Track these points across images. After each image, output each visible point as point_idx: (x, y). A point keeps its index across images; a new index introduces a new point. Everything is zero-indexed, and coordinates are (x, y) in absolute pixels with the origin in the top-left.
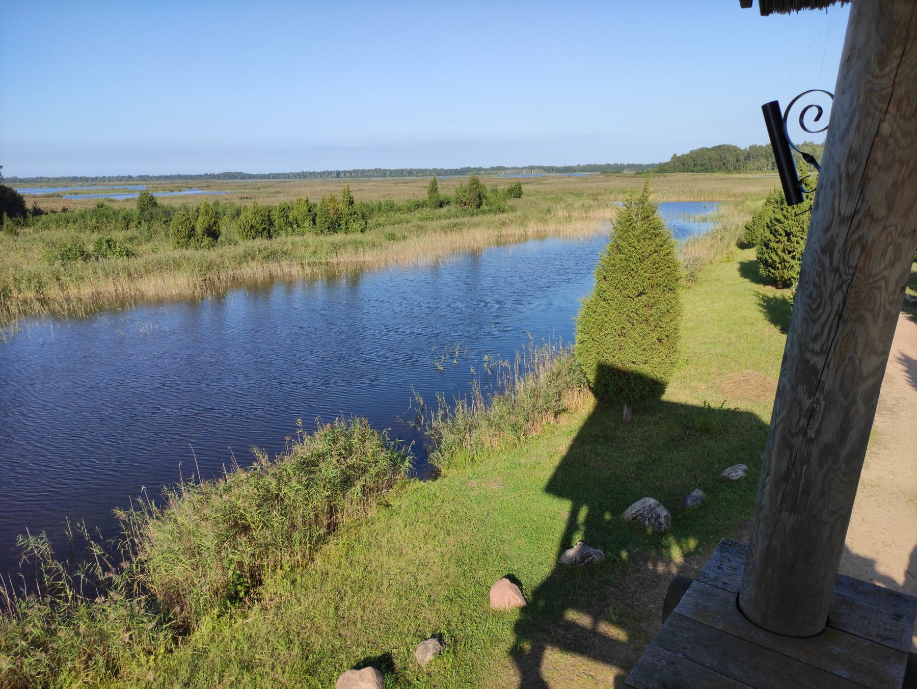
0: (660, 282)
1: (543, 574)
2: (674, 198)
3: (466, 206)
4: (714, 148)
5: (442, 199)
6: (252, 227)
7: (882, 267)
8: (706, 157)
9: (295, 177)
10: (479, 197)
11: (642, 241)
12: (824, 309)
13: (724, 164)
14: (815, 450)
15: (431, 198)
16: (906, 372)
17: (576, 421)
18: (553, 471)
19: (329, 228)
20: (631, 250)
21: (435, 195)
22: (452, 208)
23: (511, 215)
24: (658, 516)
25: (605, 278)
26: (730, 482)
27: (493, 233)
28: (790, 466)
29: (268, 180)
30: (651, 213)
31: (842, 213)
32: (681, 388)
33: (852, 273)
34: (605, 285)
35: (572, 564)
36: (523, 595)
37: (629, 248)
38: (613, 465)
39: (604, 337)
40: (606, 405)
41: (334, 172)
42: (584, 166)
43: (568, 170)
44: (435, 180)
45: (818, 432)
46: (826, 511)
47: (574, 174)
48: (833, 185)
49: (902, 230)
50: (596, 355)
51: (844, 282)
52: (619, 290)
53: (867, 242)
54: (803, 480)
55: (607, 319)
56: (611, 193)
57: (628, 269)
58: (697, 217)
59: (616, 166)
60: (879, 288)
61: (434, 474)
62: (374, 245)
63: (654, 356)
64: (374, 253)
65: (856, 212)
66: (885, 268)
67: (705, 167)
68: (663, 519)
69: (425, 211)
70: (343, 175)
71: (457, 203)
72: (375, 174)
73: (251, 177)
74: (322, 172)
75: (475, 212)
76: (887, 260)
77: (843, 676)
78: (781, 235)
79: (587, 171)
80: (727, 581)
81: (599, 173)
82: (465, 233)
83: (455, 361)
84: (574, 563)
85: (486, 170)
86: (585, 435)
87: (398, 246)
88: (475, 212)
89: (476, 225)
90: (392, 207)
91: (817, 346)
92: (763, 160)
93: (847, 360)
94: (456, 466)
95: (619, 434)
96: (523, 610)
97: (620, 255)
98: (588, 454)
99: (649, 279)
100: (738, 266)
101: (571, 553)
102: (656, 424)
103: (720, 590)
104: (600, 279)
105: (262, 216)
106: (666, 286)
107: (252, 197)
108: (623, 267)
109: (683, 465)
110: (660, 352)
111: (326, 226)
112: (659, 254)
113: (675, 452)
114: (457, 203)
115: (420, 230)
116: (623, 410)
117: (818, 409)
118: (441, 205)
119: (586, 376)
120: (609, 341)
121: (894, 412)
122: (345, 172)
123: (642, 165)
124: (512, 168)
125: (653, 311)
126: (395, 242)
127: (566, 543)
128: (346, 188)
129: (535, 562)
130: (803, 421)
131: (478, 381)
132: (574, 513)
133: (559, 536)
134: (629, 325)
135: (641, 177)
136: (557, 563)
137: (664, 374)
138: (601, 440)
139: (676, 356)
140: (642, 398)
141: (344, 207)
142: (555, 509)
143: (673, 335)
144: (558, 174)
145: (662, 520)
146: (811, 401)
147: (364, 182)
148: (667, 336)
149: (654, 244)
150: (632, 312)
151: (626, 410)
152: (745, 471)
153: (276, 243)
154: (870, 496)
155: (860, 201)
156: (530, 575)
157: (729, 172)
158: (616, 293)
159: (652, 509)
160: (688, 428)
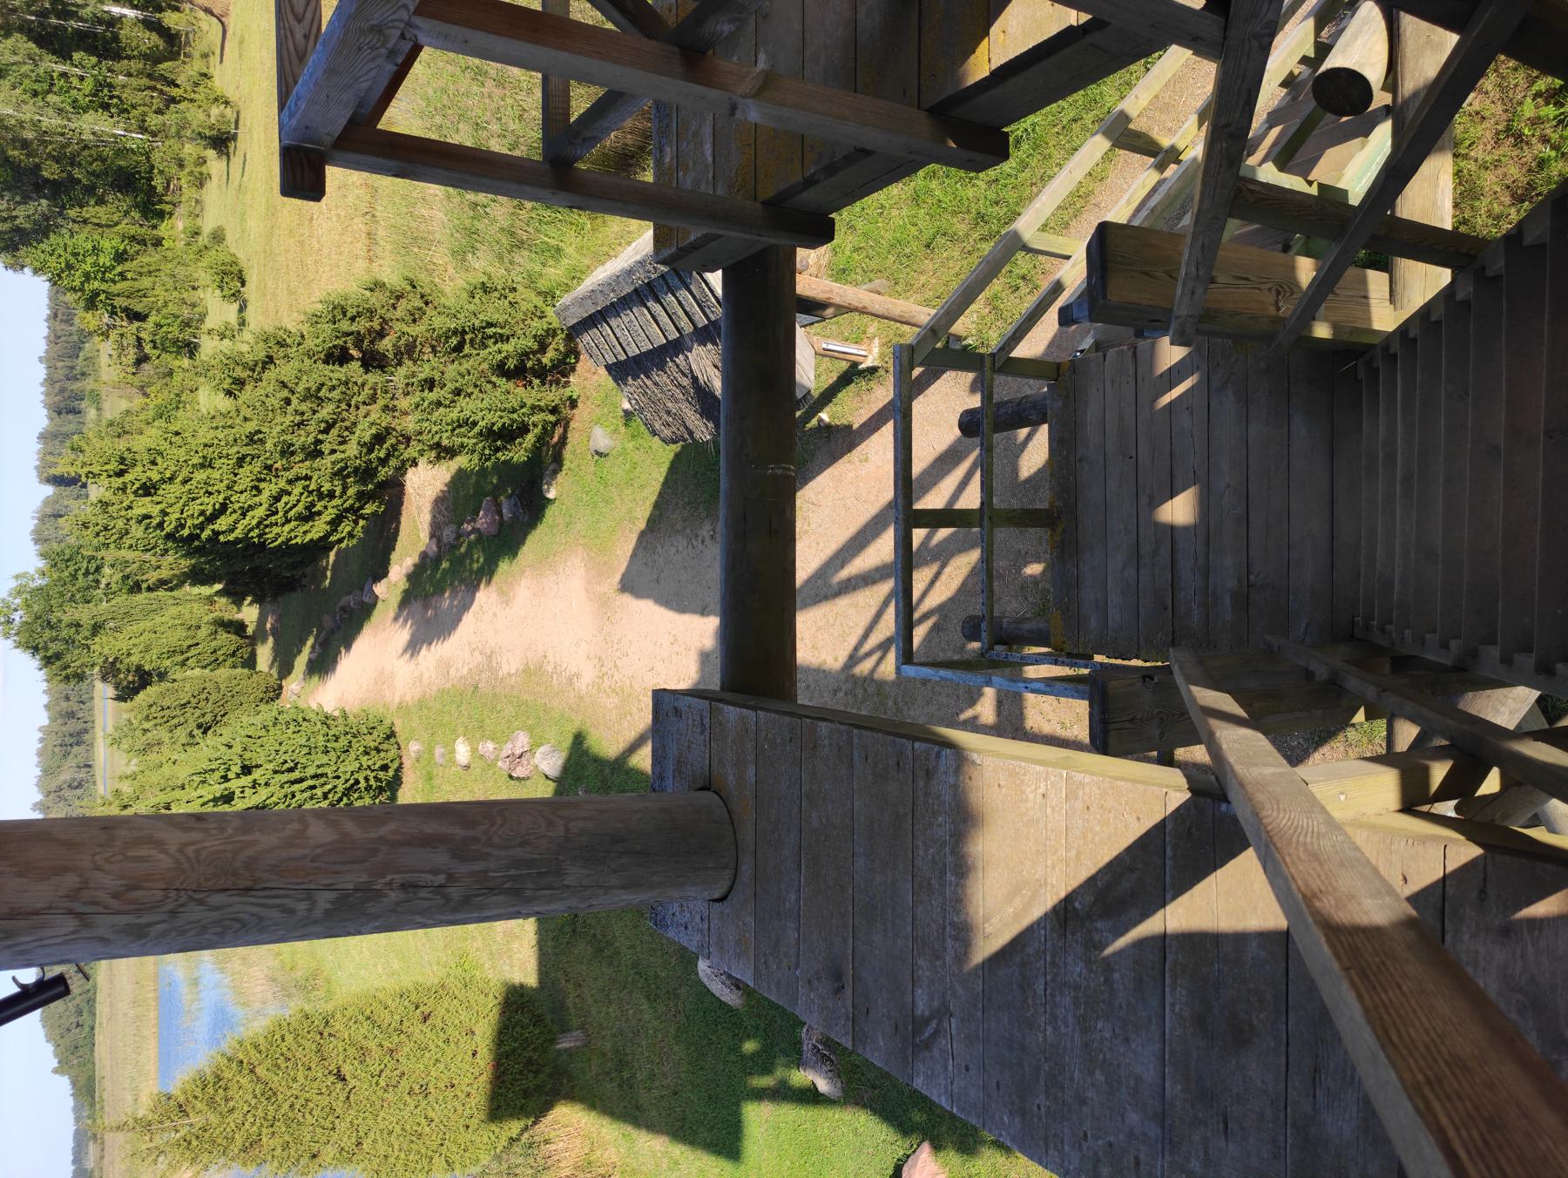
0: (314, 1046)
1: (871, 1124)
2: (151, 1050)
7: (162, 856)
11: (231, 1104)
12: (238, 913)
14: (464, 868)
16: (430, 644)
17: (604, 1130)
18: (699, 1152)
20: (252, 1120)
25: (314, 1156)
28: (496, 891)
30: (172, 1103)
31: (72, 929)
32: (510, 957)
33: (174, 892)
34: (329, 1152)
35: (839, 1076)
36: (914, 1152)
37: (247, 1126)
38: (662, 1044)
39: (433, 1124)
40: (565, 1081)
45: (435, 872)
46: (549, 834)
48: (22, 953)
49: (101, 846)
50: (470, 1130)
51: (191, 899)
52: (337, 1121)
53: (122, 886)
54: (513, 872)
55: (398, 1129)
57: (290, 1115)
60: (197, 851)
63: (457, 1022)
65: (71, 912)
66: (165, 852)
76: (153, 852)
77: (754, 772)
80: (698, 917)
84: (836, 1073)
86: (625, 1107)
91: (302, 907)
93: (317, 864)
95: (609, 1045)
96: (937, 1147)
97: (264, 1140)
98: (655, 1093)
99: (310, 1069)
101: (823, 1085)
102: (580, 985)
103: (712, 925)
104: (317, 1166)
106: (321, 1034)
108: (288, 1126)
109: (635, 927)
110: (449, 1012)
112: (256, 1063)
113: (617, 944)
116: (566, 1050)
117: (399, 881)
119: (514, 1136)
120: (439, 1113)
121: (492, 652)
125: (372, 1045)
127: (811, 1097)
129: (858, 1144)
130: (423, 894)
132: (760, 1095)
133: (803, 1112)
134: (404, 1083)
136: (845, 1103)
137: (486, 995)
138: (626, 1075)
139: (451, 982)
140: (538, 1020)
142: (762, 1130)
143: (413, 997)
146: (390, 892)
148: (417, 1007)
149: (238, 1078)
150: (377, 1084)
151: (565, 1044)
154: (616, 666)
155: (51, 911)
156: (880, 1148)
158: (342, 1126)
160: (574, 931)
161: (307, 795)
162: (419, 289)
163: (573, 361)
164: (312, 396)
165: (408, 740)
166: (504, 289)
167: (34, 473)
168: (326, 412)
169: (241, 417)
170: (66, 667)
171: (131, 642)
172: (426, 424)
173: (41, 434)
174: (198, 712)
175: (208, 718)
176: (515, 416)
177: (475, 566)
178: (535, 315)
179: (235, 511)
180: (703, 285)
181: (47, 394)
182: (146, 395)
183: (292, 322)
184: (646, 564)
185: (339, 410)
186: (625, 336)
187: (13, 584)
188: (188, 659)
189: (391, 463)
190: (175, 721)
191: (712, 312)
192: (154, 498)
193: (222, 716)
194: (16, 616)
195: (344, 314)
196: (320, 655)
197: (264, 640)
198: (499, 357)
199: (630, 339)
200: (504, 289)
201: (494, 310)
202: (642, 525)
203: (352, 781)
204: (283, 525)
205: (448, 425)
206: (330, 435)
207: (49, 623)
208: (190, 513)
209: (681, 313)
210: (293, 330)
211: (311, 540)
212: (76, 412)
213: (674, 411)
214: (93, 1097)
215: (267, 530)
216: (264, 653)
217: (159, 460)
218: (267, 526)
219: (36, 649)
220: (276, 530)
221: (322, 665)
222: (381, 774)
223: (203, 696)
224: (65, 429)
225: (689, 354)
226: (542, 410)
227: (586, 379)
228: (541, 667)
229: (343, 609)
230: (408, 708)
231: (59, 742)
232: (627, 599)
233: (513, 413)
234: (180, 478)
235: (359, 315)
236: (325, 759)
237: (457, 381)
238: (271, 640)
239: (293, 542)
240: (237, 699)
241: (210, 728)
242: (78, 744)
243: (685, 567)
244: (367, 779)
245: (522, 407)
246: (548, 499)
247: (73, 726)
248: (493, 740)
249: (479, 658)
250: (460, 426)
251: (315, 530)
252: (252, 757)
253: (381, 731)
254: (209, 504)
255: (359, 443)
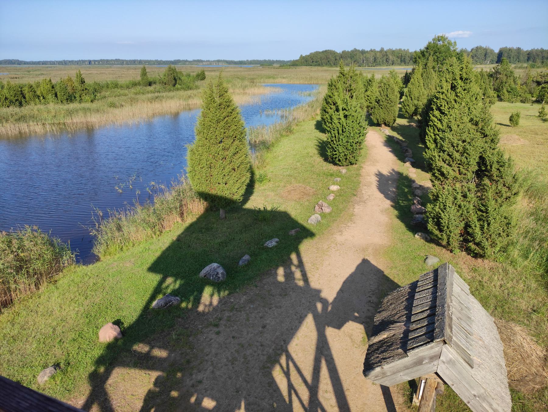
3: (166, 85)
4: (323, 52)
5: (151, 80)
6: (6, 99)
8: (319, 57)
9: (59, 64)
10: (175, 79)
13: (328, 61)
15: (142, 79)
16: (378, 181)
19: (67, 99)
21: (146, 78)
22: (158, 86)
23: (195, 92)
24: (218, 273)
26: (267, 249)
27: (183, 103)
29: (38, 66)
35: (159, 308)
41: (86, 61)
42: (250, 61)
43: (241, 63)
44: (144, 68)
47: (245, 65)
56: (261, 78)
58: (306, 93)
59: (269, 61)
61: (95, 259)
62: (98, 111)
64: (98, 116)
67: (318, 63)
68: (220, 275)
69: (138, 88)
70: (93, 63)
71: (160, 83)
72: (116, 63)
73: (25, 63)
74: (78, 61)
75: (172, 89)
78: (331, 104)
79: (253, 64)
81: (259, 65)
82: (164, 102)
83: (131, 186)
85: (190, 62)
87: (117, 111)
88: (172, 89)
89: (172, 98)
90: (116, 85)
92: (349, 60)
94: (110, 254)
100: (315, 123)
105: (15, 91)
107: (20, 77)
111: (65, 98)
114: (160, 83)
115: (133, 101)
118: (150, 84)
122: (95, 61)
123: (284, 61)
124: (207, 61)
126: (114, 109)
127: (153, 298)
128: (78, 72)
131: (137, 200)
135: (282, 68)
141: (78, 85)
144: (235, 65)
145: (220, 275)
147: (107, 68)
152: (277, 242)
153: (26, 110)
154: (337, 250)
157: (331, 66)
159: (215, 270)
161: (333, 135)
162: (512, 196)
163: (472, 255)
164: (465, 151)
165: (347, 169)
166: (507, 232)
167: (504, 46)
168: (457, 155)
169: (460, 124)
170: (419, 58)
171: (416, 79)
172: (447, 193)
173: (520, 48)
174: (384, 100)
175: (381, 103)
176: (446, 228)
177: (401, 202)
178: (493, 243)
179: (441, 117)
180: (422, 343)
181: (537, 50)
182: (522, 85)
183: (501, 145)
184: (371, 270)
185: (457, 160)
186: (423, 294)
187: (453, 41)
188: (407, 97)
189: (433, 177)
190: (382, 92)
191: (411, 343)
192: (450, 89)
193: (381, 108)
194: (441, 43)
195: (501, 166)
196: (394, 140)
197: (409, 122)
198: (473, 226)
199: (421, 296)
200: (507, 232)
201: (495, 226)
202: (386, 273)
203: (335, 149)
204: (433, 133)
205: (445, 201)
206: (446, 156)
207: (436, 53)
208: (442, 102)
209: (419, 326)
210: (497, 145)
211: (426, 143)
212: (528, 60)
213: (390, 307)
214: (292, 66)
215: (432, 128)
216: (403, 122)
217: (466, 92)
218: (434, 127)
219: (427, 48)
220: (432, 131)
221: (390, 142)
222: (337, 159)
223: (389, 102)
224: (521, 56)
225: (403, 323)
226: (448, 239)
227: (463, 259)
228: (351, 221)
229: (407, 150)
230: (359, 170)
231: (403, 55)
232: (359, 261)
233: (447, 227)
234: (456, 98)
235: (500, 172)
236: (344, 142)
237: (464, 207)
238: (408, 124)
239: (427, 136)
240: (387, 113)
241: (378, 103)
242: (401, 61)
243: (362, 287)
244: (336, 154)
245: (450, 231)
246: (415, 234)
247: (407, 59)
248: (334, 199)
249: (366, 197)
250: (444, 206)
251: (430, 144)
252: (350, 119)
253: (353, 161)
254: (445, 109)
255: (442, 166)
